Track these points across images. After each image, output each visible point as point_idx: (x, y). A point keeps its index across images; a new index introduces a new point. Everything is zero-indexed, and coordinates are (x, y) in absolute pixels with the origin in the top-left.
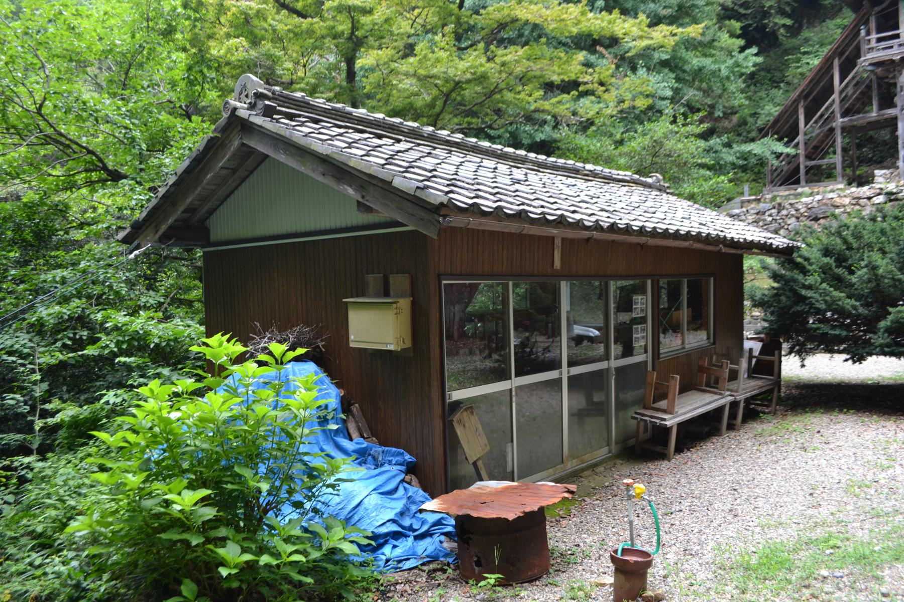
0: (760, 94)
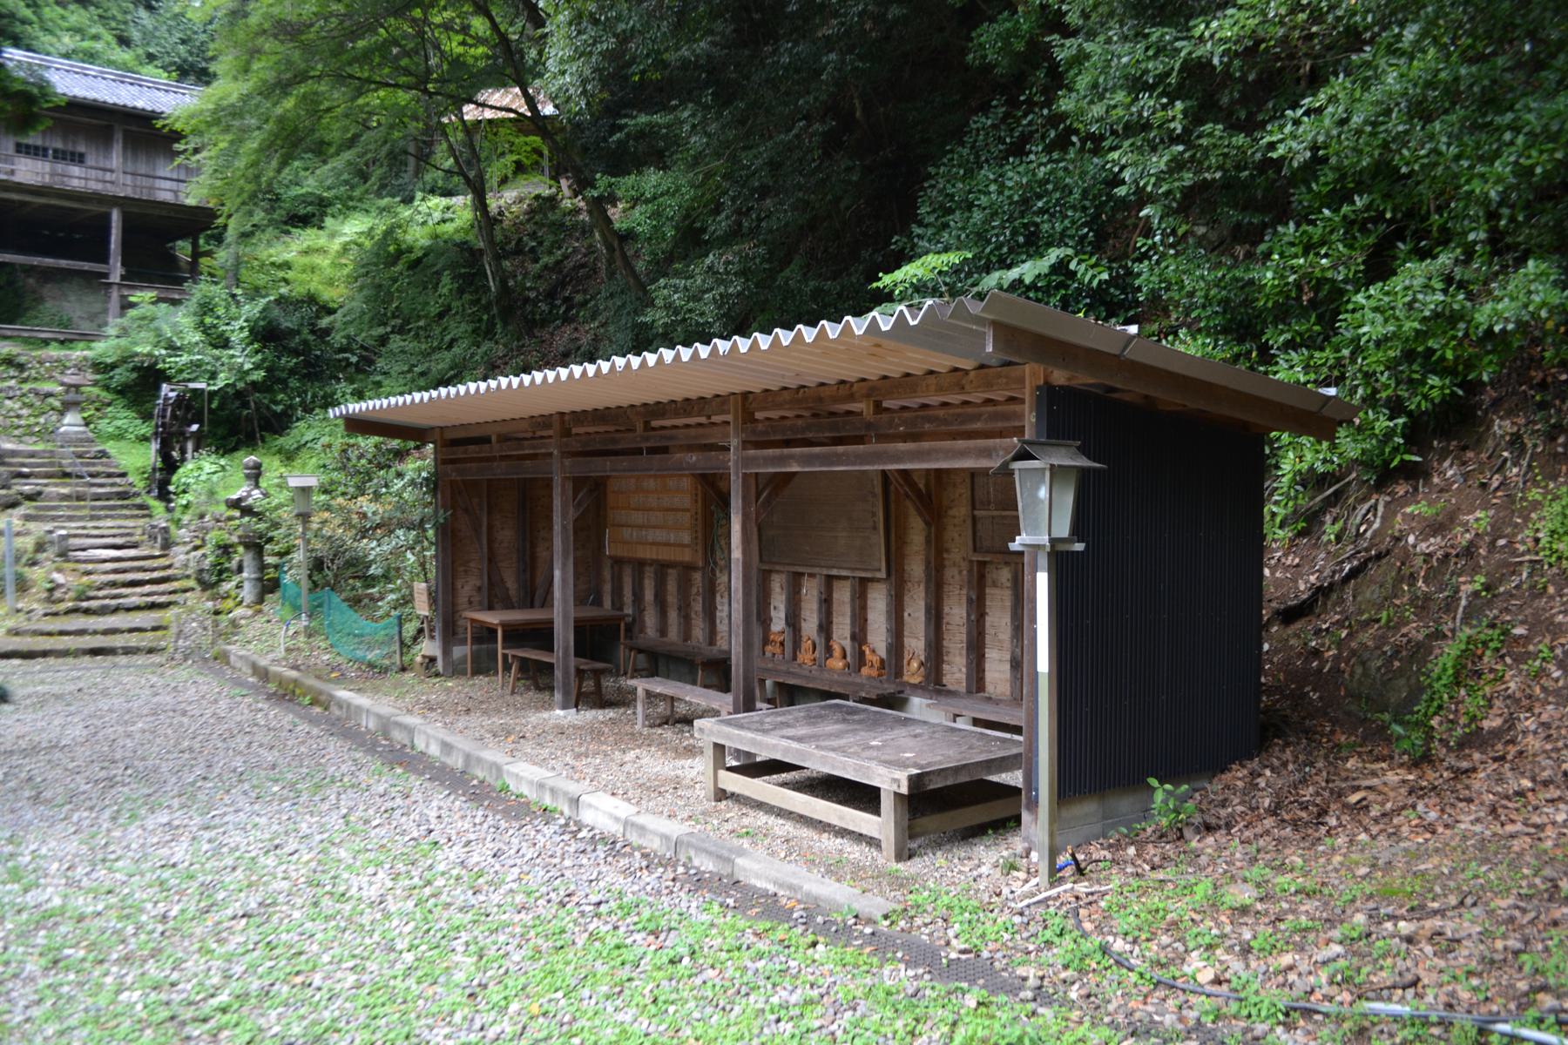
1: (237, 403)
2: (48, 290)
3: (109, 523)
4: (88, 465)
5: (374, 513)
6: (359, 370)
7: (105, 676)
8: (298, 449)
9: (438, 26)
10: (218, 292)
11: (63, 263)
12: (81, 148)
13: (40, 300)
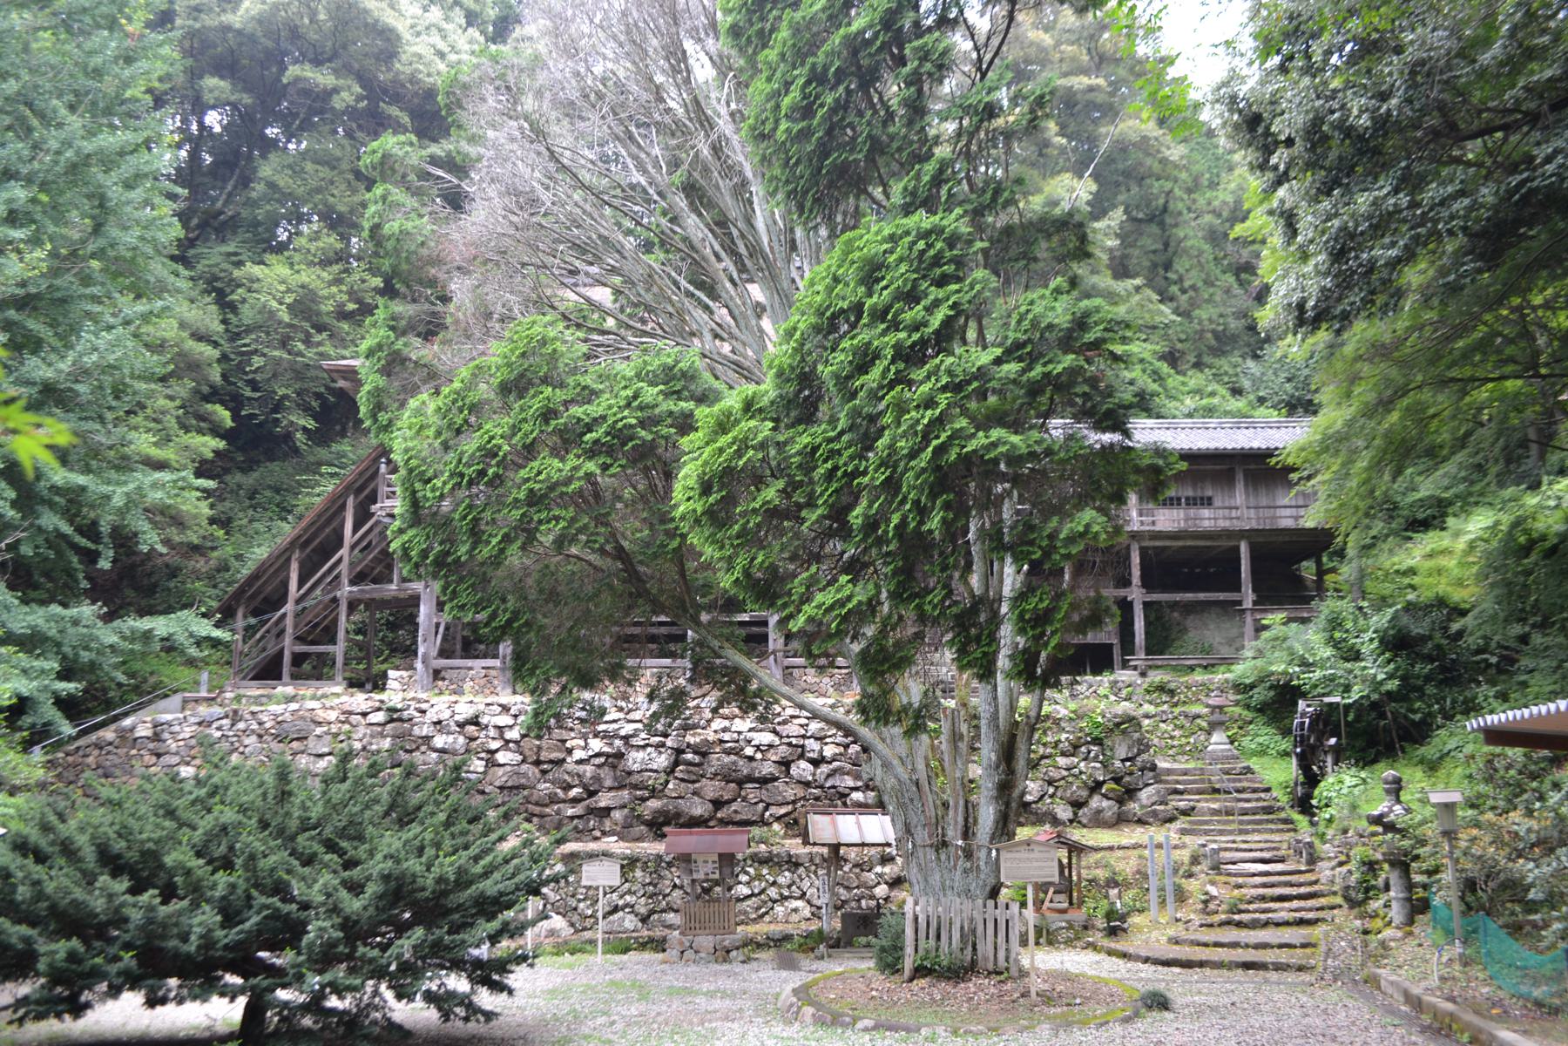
0: (256, 525)
1: (1374, 715)
2: (1190, 621)
3: (1257, 837)
4: (1234, 781)
5: (1529, 830)
6: (1500, 671)
7: (1258, 991)
8: (1441, 758)
9: (1540, 306)
10: (1345, 607)
11: (1202, 596)
12: (1209, 493)
13: (1184, 631)
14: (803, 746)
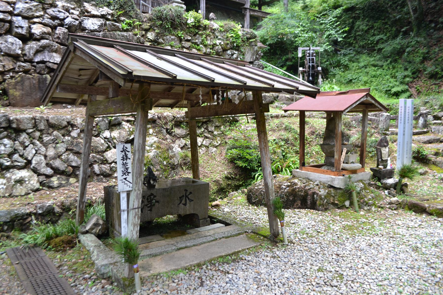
14: (10, 22)
